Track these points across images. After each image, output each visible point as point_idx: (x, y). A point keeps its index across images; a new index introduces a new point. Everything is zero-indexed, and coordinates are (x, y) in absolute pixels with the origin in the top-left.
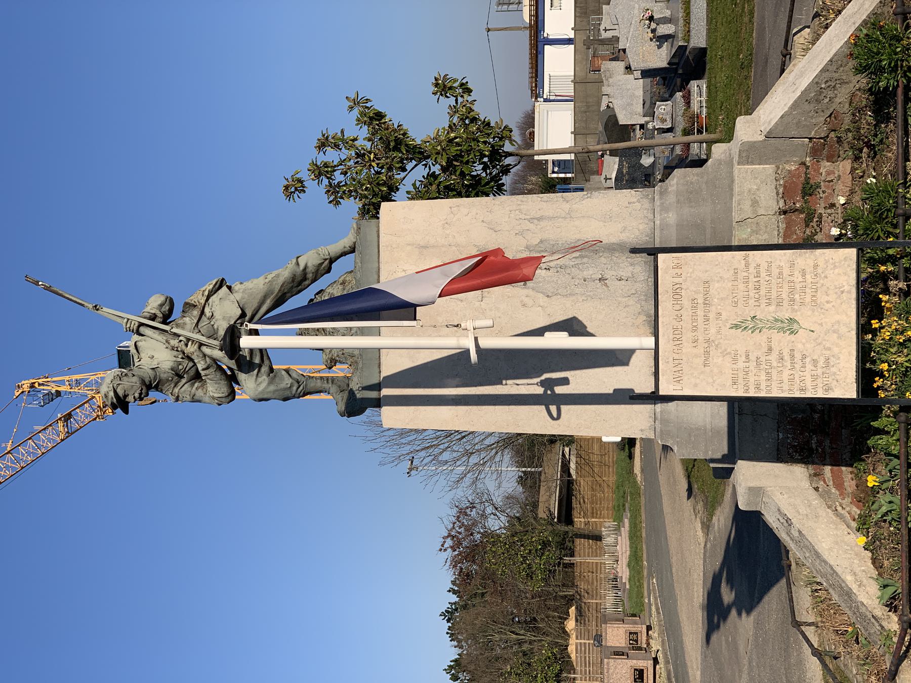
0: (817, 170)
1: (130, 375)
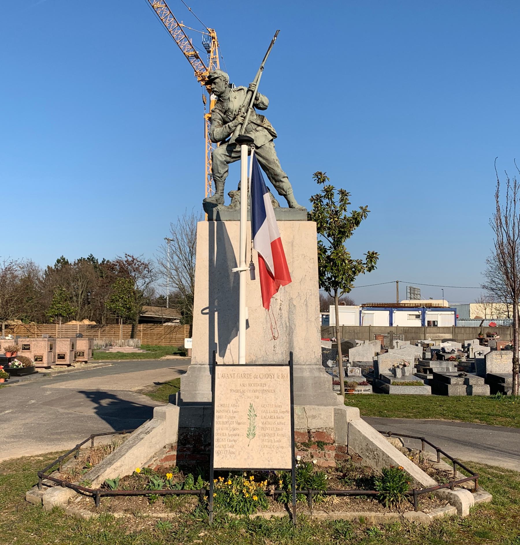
1: (226, 86)
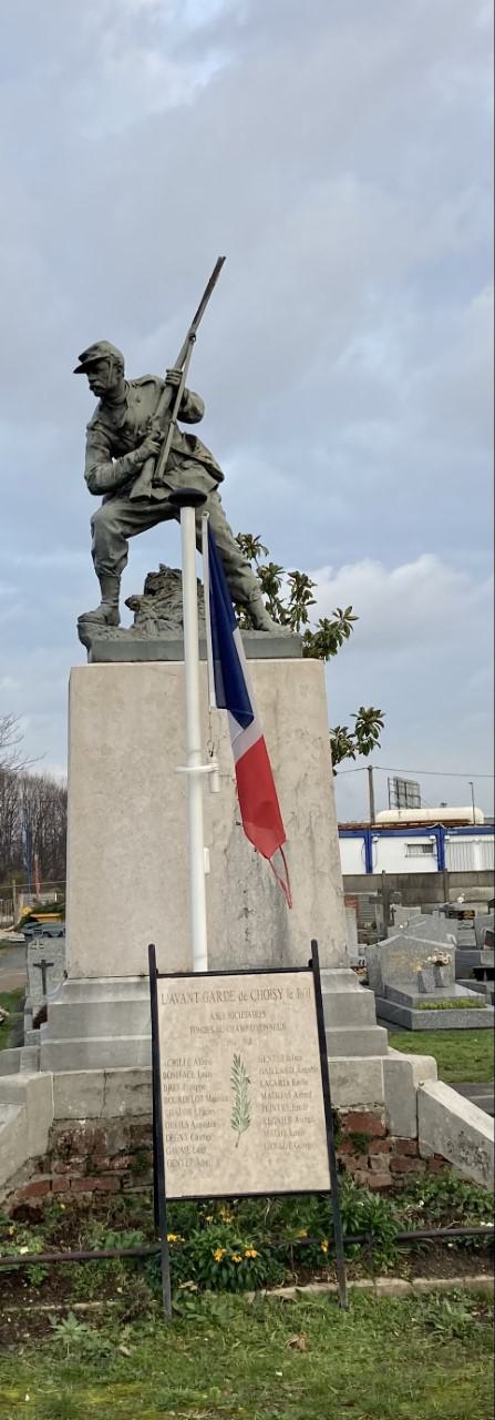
0: (380, 1149)
